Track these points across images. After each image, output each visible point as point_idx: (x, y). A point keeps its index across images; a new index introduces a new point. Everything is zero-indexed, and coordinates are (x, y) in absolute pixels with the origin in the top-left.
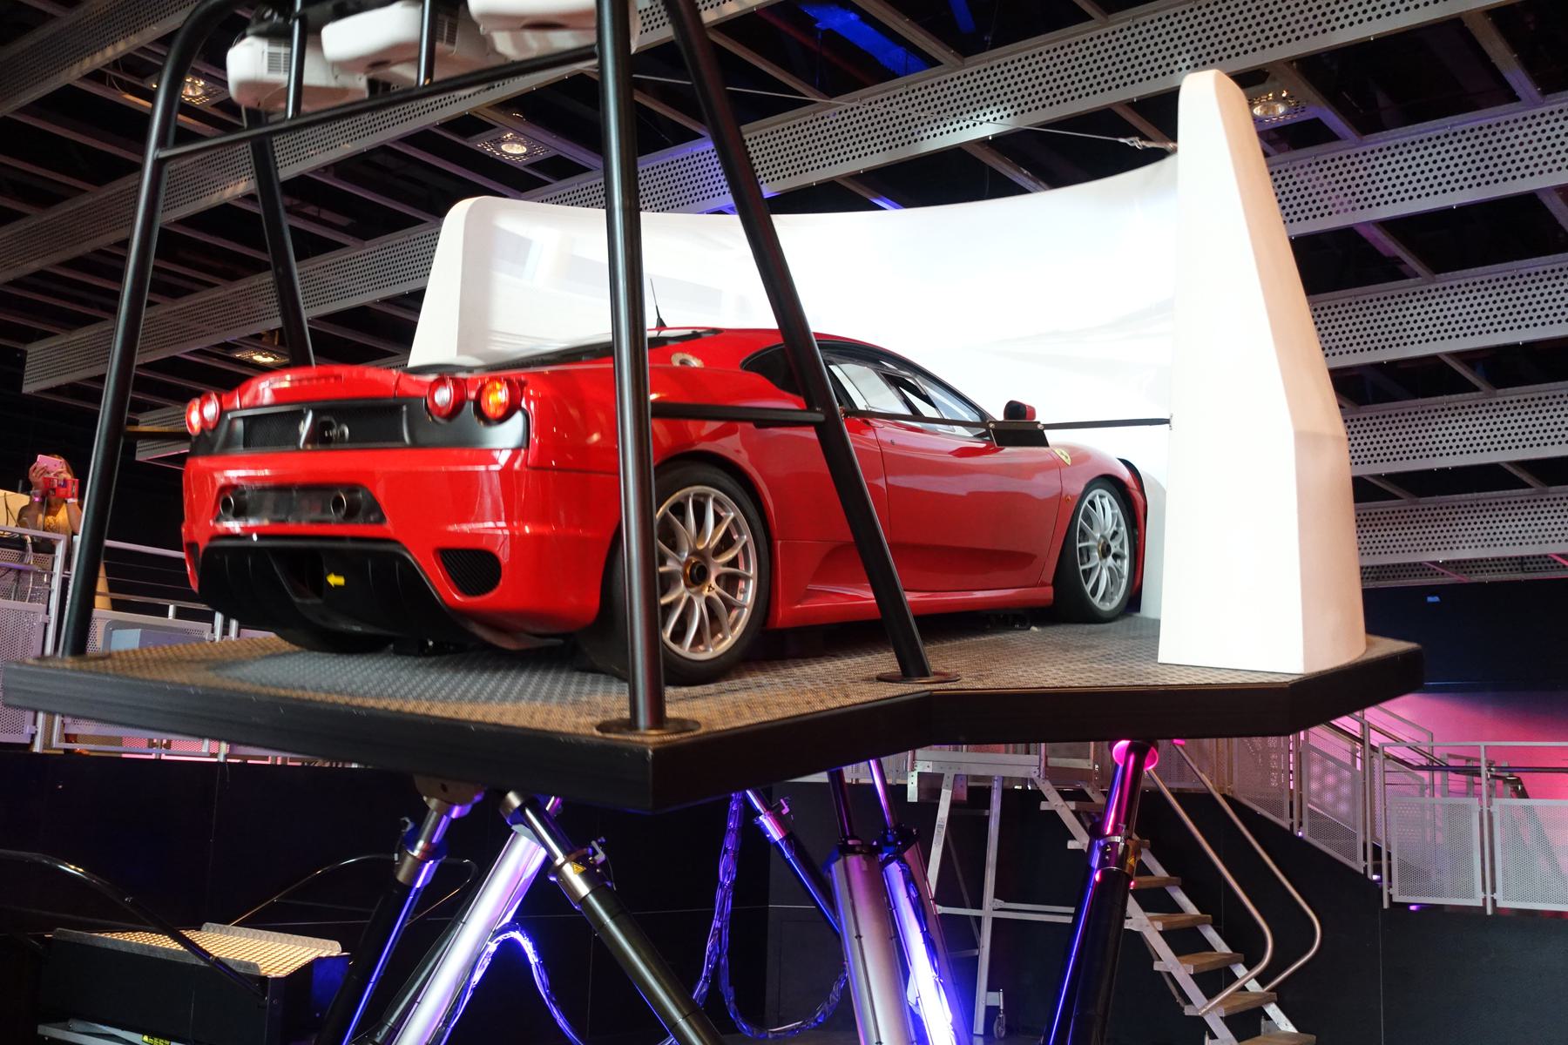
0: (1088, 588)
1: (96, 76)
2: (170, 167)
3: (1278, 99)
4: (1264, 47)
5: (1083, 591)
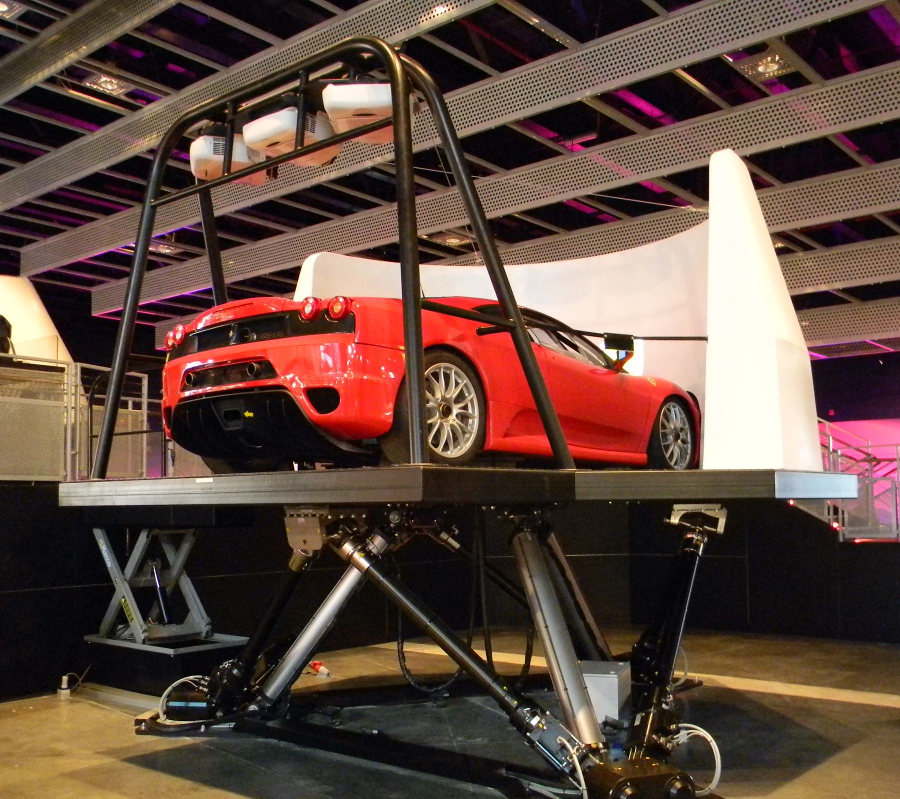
0: (667, 456)
1: (51, 80)
2: (159, 209)
3: (773, 61)
4: (764, 29)
5: (664, 456)
